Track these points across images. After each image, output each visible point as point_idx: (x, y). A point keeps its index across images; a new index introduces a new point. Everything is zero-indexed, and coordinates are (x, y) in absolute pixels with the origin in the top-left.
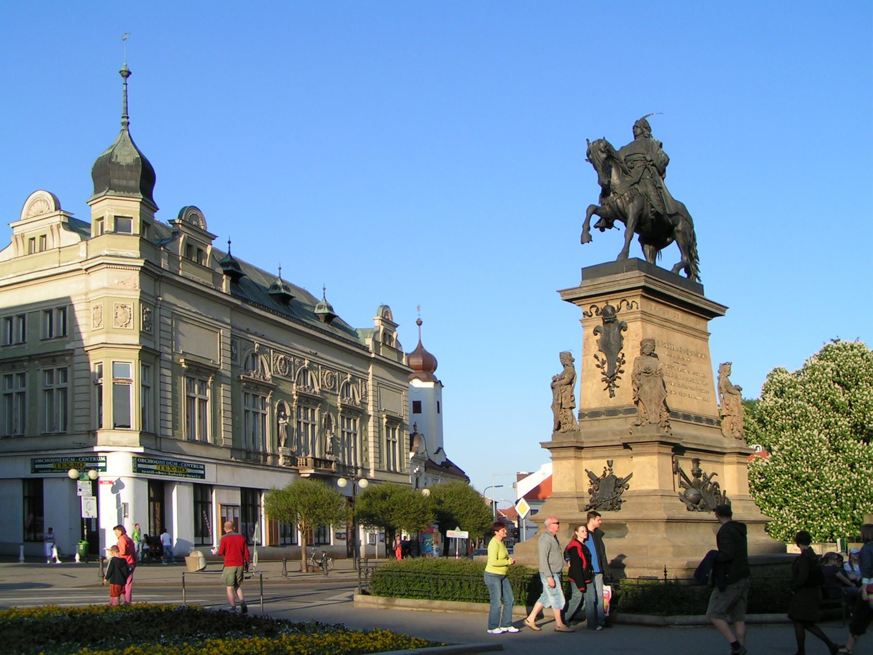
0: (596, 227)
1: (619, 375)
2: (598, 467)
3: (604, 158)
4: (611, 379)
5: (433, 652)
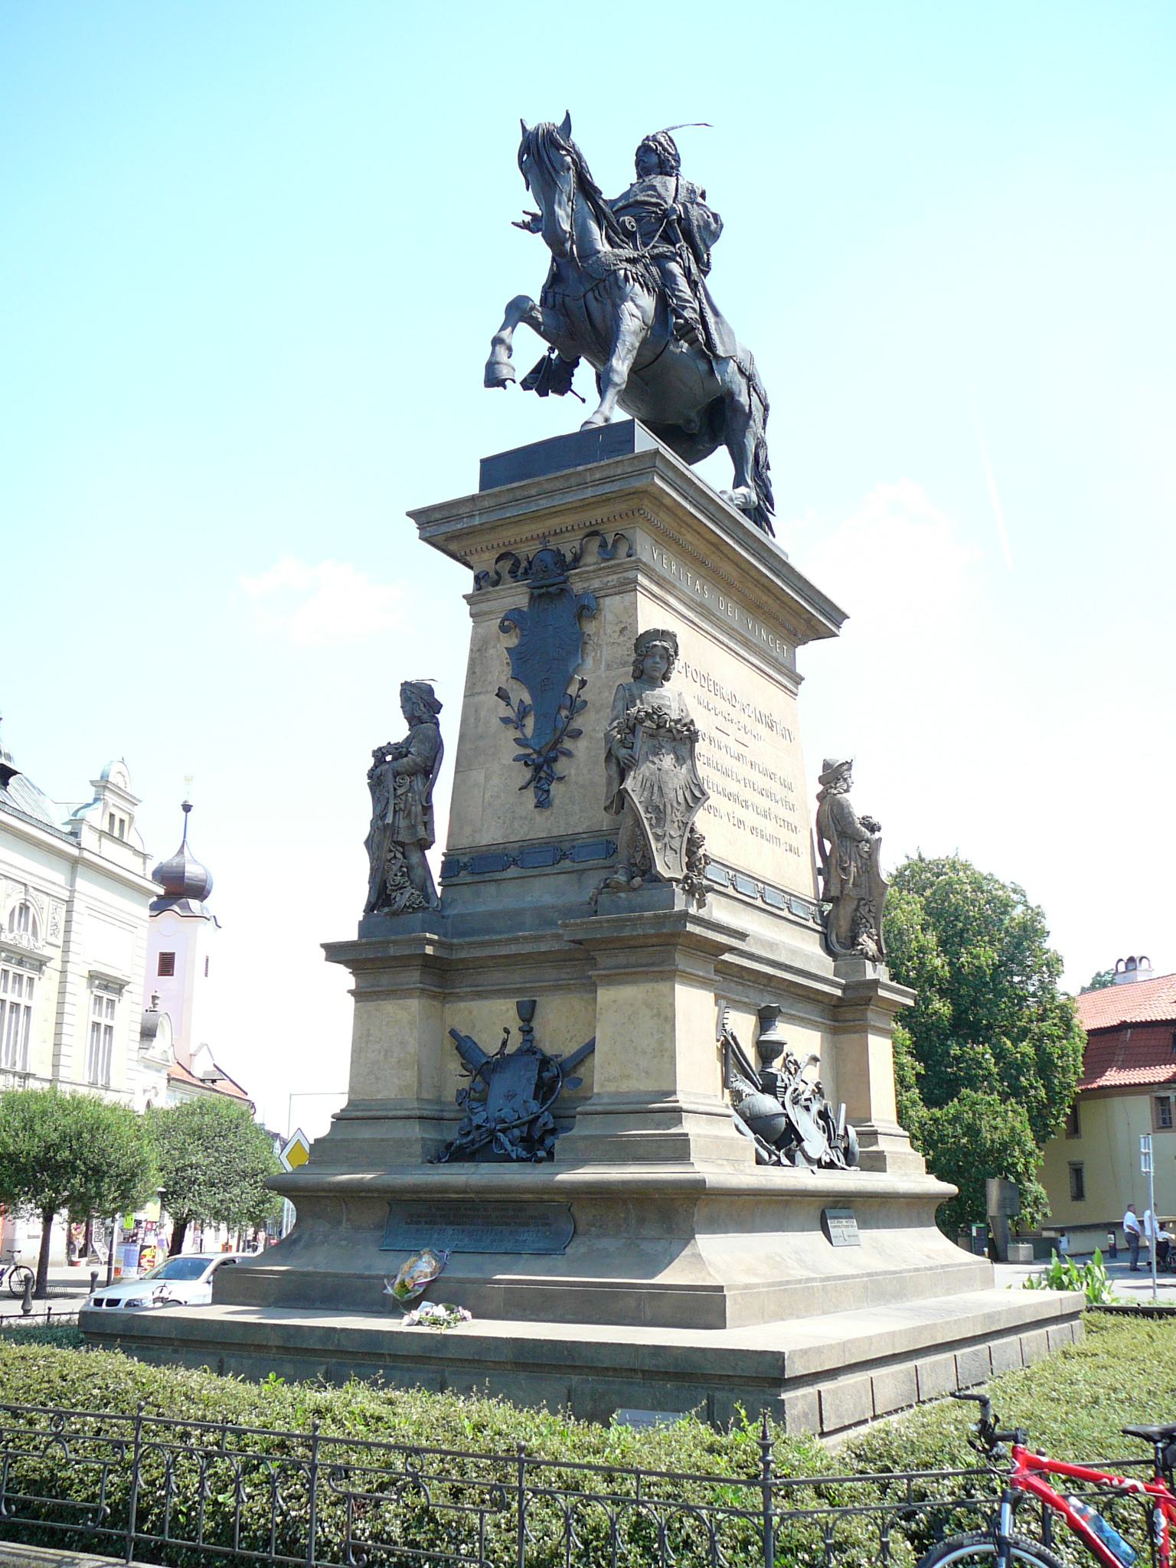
1: (568, 744)
2: (492, 1021)
4: (542, 768)
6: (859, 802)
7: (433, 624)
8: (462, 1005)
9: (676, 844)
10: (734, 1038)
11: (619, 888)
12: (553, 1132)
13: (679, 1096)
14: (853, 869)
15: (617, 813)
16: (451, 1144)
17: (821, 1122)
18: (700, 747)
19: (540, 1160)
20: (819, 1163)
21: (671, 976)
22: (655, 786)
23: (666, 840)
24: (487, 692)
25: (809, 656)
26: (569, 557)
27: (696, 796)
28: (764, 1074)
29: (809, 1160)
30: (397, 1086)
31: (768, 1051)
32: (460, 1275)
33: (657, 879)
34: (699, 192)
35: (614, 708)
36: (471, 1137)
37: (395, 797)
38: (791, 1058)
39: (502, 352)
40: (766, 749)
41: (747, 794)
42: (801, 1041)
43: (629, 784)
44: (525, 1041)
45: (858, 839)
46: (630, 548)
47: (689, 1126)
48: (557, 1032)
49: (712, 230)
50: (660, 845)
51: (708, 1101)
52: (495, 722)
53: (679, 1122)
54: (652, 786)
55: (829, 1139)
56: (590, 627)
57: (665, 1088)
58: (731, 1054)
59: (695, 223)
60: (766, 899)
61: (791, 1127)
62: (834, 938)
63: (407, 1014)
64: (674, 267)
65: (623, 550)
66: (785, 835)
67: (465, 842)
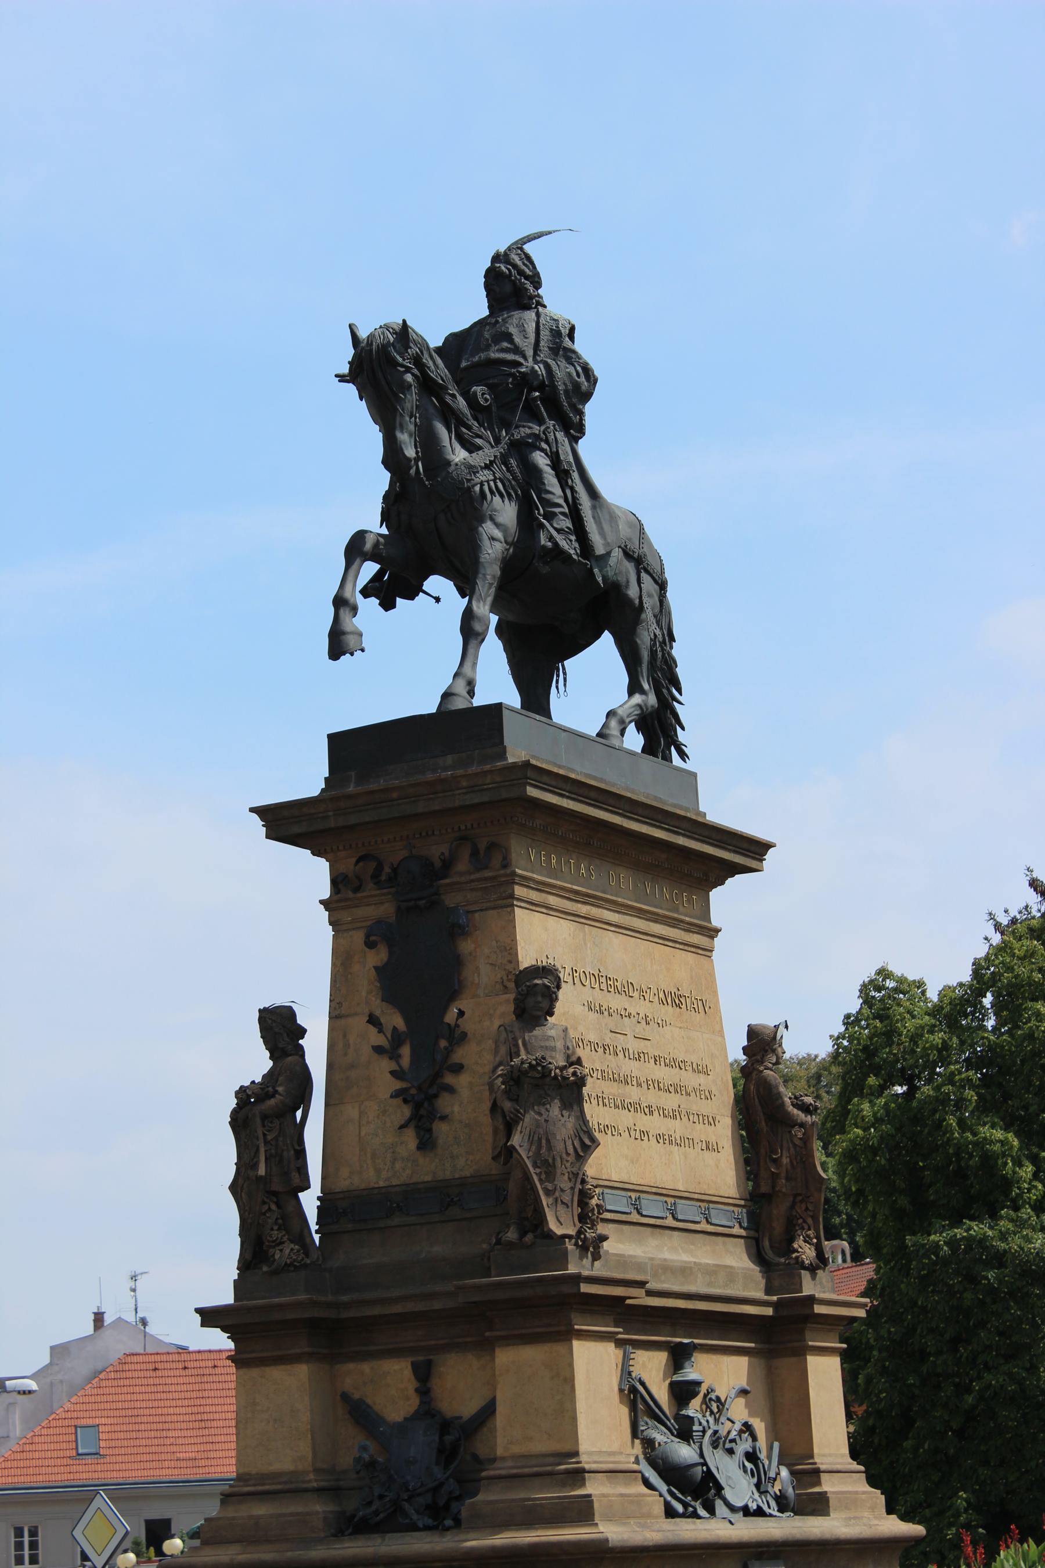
1: (449, 1079)
3: (380, 368)
4: (423, 1105)
7: (282, 933)
8: (351, 1366)
9: (566, 1198)
10: (643, 1384)
11: (511, 1245)
12: (459, 1498)
13: (583, 1458)
14: (785, 1161)
15: (506, 1163)
16: (353, 1516)
20: (746, 1511)
21: (567, 1335)
22: (541, 1140)
23: (557, 1194)
24: (356, 1014)
25: (727, 900)
26: (438, 864)
27: (586, 1142)
28: (678, 1417)
30: (291, 1455)
31: (683, 1392)
33: (550, 1235)
34: (565, 331)
35: (496, 1052)
36: (374, 1508)
37: (266, 1142)
38: (713, 1396)
39: (345, 614)
40: (673, 1037)
41: (651, 1097)
42: (724, 1373)
43: (516, 1140)
44: (422, 1403)
46: (505, 858)
47: (593, 1488)
48: (460, 1386)
50: (551, 1200)
51: (611, 1459)
52: (366, 1051)
53: (582, 1483)
54: (540, 1139)
55: (758, 1486)
56: (466, 946)
57: (567, 1447)
58: (639, 1400)
60: (674, 1213)
61: (709, 1475)
62: (766, 1243)
63: (293, 1384)
64: (541, 460)
65: (496, 861)
66: (701, 1132)
67: (343, 1183)
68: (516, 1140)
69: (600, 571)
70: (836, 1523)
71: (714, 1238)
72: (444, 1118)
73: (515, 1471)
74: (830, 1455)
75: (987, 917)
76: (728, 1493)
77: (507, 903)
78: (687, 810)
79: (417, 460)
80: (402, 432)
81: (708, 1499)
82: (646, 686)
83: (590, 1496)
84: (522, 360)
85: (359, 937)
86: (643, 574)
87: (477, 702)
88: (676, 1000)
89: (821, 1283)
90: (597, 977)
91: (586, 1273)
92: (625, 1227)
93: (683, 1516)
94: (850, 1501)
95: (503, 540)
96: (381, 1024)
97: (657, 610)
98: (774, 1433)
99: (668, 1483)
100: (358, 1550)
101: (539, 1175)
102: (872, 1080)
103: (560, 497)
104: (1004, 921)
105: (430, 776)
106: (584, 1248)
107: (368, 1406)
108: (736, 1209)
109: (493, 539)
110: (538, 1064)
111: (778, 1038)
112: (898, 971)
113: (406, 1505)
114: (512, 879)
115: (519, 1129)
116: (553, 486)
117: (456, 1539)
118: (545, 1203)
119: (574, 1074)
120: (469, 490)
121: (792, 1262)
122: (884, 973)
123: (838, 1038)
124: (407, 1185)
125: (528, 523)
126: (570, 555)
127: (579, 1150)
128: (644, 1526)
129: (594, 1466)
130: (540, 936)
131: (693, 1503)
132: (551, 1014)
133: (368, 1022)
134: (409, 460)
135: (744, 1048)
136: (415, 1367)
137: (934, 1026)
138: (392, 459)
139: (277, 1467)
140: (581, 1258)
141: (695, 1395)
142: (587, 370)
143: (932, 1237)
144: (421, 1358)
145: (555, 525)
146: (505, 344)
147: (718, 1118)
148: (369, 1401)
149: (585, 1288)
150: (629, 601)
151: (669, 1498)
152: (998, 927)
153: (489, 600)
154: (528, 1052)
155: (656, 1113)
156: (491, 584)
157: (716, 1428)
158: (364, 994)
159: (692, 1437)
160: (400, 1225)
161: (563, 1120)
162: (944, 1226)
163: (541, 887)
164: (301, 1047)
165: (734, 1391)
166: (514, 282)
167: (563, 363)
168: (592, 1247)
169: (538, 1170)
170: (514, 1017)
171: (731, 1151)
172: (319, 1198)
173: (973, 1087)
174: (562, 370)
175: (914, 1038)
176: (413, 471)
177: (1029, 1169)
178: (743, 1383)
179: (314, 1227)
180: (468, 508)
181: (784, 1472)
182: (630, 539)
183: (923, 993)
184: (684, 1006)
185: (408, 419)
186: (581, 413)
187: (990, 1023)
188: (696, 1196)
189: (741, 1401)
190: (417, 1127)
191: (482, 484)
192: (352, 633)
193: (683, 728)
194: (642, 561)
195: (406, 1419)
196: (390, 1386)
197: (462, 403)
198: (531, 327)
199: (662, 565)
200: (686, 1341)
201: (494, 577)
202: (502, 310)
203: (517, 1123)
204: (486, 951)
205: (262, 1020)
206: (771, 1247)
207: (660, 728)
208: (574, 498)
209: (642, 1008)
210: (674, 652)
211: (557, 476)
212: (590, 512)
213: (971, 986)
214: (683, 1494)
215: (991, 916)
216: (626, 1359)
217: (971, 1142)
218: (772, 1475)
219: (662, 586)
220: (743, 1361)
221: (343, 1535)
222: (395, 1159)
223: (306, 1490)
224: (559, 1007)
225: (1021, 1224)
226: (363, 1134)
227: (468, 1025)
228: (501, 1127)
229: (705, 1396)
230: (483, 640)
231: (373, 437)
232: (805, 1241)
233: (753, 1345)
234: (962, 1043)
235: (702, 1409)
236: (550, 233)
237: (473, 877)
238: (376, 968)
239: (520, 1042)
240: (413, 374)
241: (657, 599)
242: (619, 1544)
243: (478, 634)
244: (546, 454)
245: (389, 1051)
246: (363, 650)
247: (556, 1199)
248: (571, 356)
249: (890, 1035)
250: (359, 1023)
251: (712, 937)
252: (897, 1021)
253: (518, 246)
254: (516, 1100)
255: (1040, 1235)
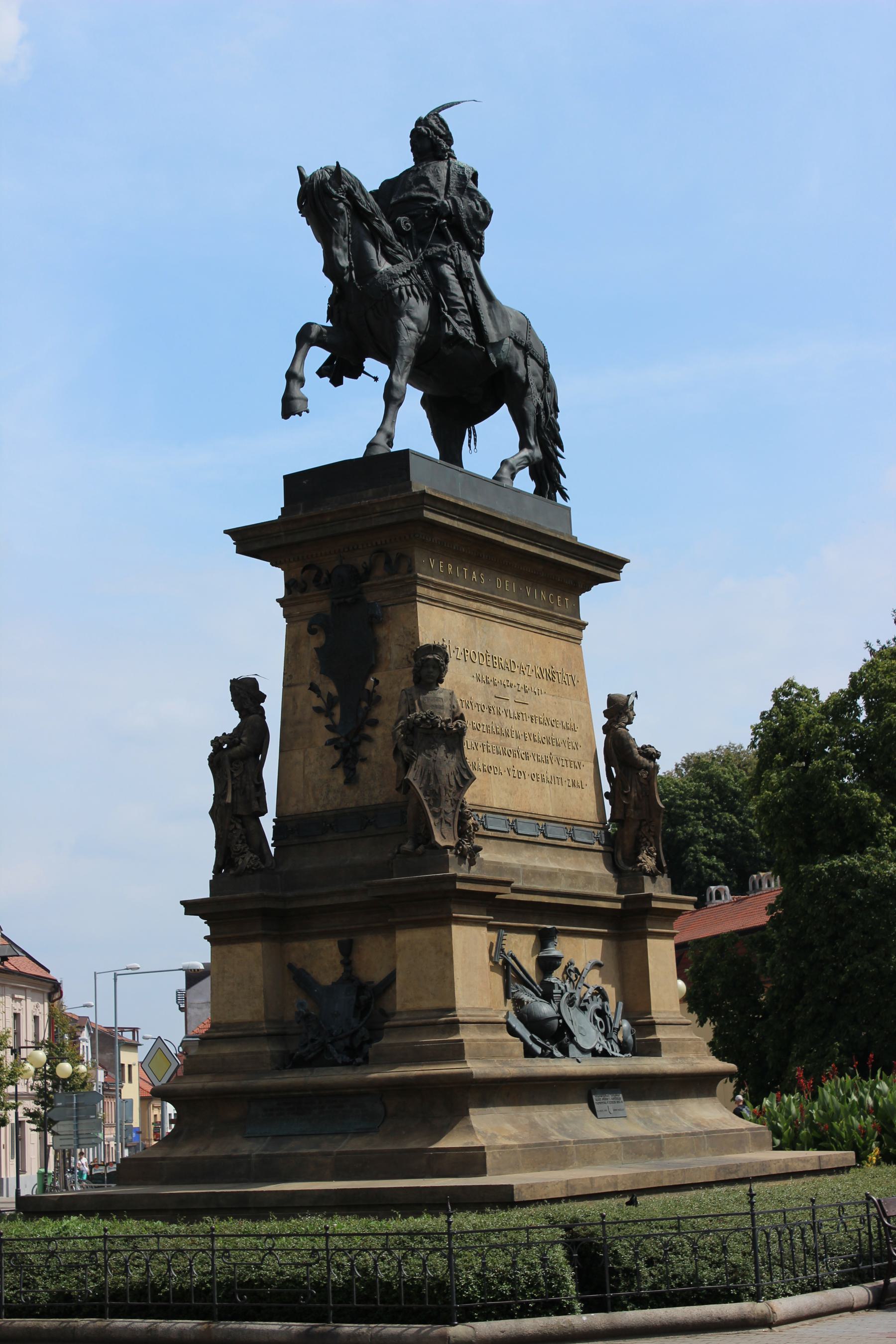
0: (321, 373)
1: (368, 731)
3: (324, 199)
4: (349, 750)
5: (37, 1330)
6: (639, 733)
7: (250, 623)
8: (296, 944)
10: (514, 958)
11: (407, 854)
12: (370, 1042)
13: (459, 1013)
14: (634, 795)
16: (293, 1054)
17: (598, 1019)
18: (470, 738)
19: (359, 1065)
20: (594, 1053)
21: (447, 921)
22: (431, 775)
23: (442, 816)
25: (593, 603)
27: (465, 777)
28: (543, 983)
29: (583, 1051)
30: (249, 1010)
31: (547, 965)
32: (305, 1151)
33: (436, 846)
34: (469, 176)
35: (399, 709)
36: (307, 1049)
37: (233, 779)
38: (572, 968)
39: (295, 385)
40: (546, 702)
41: (528, 747)
43: (411, 775)
45: (639, 767)
46: (410, 566)
47: (465, 1035)
48: (372, 960)
49: (482, 217)
50: (437, 820)
52: (309, 710)
53: (457, 1031)
54: (429, 775)
56: (382, 632)
57: (447, 1004)
58: (510, 969)
59: (464, 217)
60: (546, 832)
61: (564, 1027)
62: (619, 856)
63: (251, 956)
64: (448, 271)
66: (568, 773)
67: (291, 810)
68: (411, 775)
69: (495, 355)
70: (664, 1062)
71: (577, 851)
72: (364, 760)
73: (409, 1022)
74: (665, 1012)
75: (865, 646)
76: (580, 1040)
77: (411, 599)
78: (562, 534)
79: (350, 268)
80: (337, 247)
81: (562, 1044)
82: (532, 443)
83: (462, 1040)
84: (435, 197)
85: (304, 626)
86: (529, 359)
87: (392, 450)
88: (551, 676)
89: (660, 886)
90: (485, 656)
91: (460, 874)
92: (503, 842)
93: (542, 1055)
94: (678, 1046)
95: (416, 329)
96: (319, 691)
97: (541, 386)
98: (622, 995)
99: (531, 1031)
100: (294, 1080)
101: (428, 801)
102: (778, 757)
103: (461, 298)
104: (877, 648)
105: (355, 504)
106: (462, 856)
107: (308, 974)
108: (596, 831)
109: (409, 329)
110: (427, 718)
111: (630, 703)
112: (800, 682)
113: (330, 1046)
114: (415, 581)
115: (413, 767)
116: (456, 290)
117: (365, 1071)
118: (432, 823)
119: (457, 726)
120: (391, 292)
121: (637, 869)
122: (791, 684)
123: (756, 728)
124: (337, 810)
125: (436, 317)
126: (467, 342)
127: (460, 783)
128: (505, 1063)
129: (467, 1019)
130: (435, 623)
131: (550, 1047)
132: (442, 682)
133: (310, 689)
134: (343, 268)
135: (605, 712)
136: (341, 945)
137: (822, 719)
138: (331, 269)
139: (239, 1018)
140: (460, 864)
141: (556, 967)
142: (485, 204)
143: (817, 866)
144: (345, 938)
145: (457, 319)
146: (423, 186)
147: (583, 763)
148: (308, 970)
149: (459, 886)
150: (519, 379)
151: (531, 1043)
152: (872, 652)
153: (406, 375)
154: (422, 709)
155: (531, 759)
156: (407, 363)
157: (572, 991)
158: (308, 668)
159: (552, 997)
160: (335, 838)
161: (447, 761)
162: (826, 858)
163: (438, 588)
164: (262, 709)
165: (590, 965)
166: (431, 140)
167: (466, 199)
168: (470, 855)
169: (428, 798)
170: (413, 684)
171: (593, 787)
172: (274, 820)
173: (851, 761)
174: (464, 204)
175: (808, 728)
176: (347, 277)
177: (888, 818)
178: (598, 959)
179: (270, 841)
180: (390, 306)
181: (626, 1025)
182: (519, 332)
183: (817, 697)
184: (556, 680)
185: (342, 237)
186: (481, 237)
187: (863, 717)
188: (563, 820)
189: (596, 972)
190: (345, 767)
191: (400, 287)
192: (299, 398)
193: (565, 476)
194: (528, 347)
195: (333, 983)
196: (323, 959)
197: (388, 228)
198: (443, 174)
199: (545, 353)
200: (549, 927)
201: (409, 357)
202: (422, 161)
203: (412, 762)
204: (396, 635)
205: (232, 688)
206: (623, 858)
207: (548, 475)
208: (474, 300)
209: (522, 680)
210: (558, 420)
211: (460, 283)
212: (487, 311)
213: (848, 692)
214: (543, 1039)
215: (868, 645)
216: (500, 939)
217: (847, 800)
218: (617, 1026)
219: (545, 368)
220: (598, 943)
221: (284, 1068)
222: (329, 791)
223: (259, 1035)
224: (447, 678)
225: (881, 856)
226: (306, 772)
227: (383, 690)
228: (401, 766)
229: (566, 967)
230: (400, 405)
231: (317, 250)
232: (648, 854)
233: (606, 931)
234: (841, 731)
235: (563, 978)
236: (459, 103)
237: (386, 580)
238: (316, 649)
239: (416, 702)
240: (345, 204)
241: (540, 377)
242: (482, 1077)
243: (396, 400)
244: (452, 266)
245: (325, 711)
246: (308, 412)
247: (441, 820)
248: (473, 194)
249: (793, 725)
250: (304, 690)
251: (581, 630)
252: (797, 716)
253: (435, 113)
254: (410, 745)
255: (893, 864)
